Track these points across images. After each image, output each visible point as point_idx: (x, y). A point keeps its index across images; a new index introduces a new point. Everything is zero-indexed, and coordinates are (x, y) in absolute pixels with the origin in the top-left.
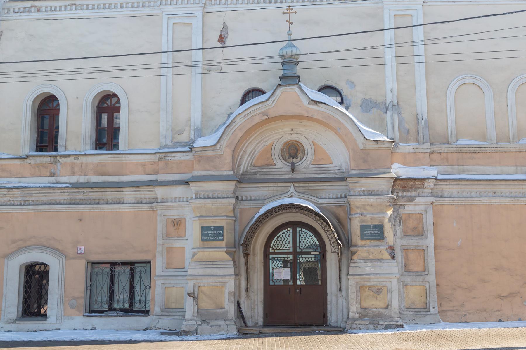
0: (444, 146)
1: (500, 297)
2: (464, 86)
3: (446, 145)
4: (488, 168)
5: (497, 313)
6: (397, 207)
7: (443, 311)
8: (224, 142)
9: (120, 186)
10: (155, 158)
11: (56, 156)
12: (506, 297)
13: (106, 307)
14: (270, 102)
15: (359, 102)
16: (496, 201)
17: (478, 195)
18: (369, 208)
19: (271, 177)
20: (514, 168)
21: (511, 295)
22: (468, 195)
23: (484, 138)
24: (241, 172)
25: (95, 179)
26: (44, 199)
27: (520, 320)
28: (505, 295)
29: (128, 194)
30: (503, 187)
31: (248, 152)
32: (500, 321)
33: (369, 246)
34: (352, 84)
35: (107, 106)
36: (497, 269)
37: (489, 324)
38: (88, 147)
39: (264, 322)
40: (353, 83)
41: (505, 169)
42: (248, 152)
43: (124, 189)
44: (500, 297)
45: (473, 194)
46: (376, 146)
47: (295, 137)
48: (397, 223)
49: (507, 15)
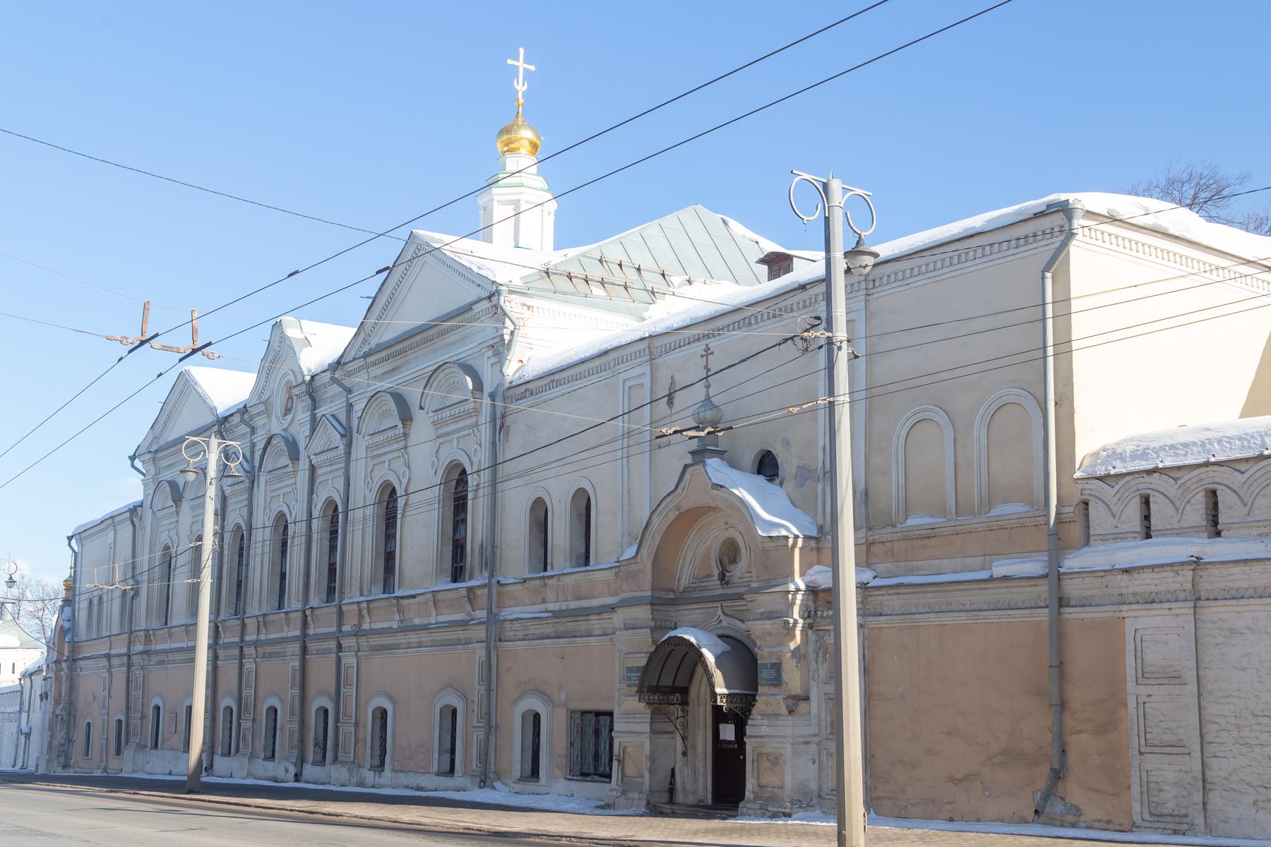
0: (885, 531)
1: (953, 780)
2: (918, 426)
3: (889, 529)
4: (945, 562)
5: (949, 807)
6: (821, 633)
7: (878, 798)
8: (644, 551)
9: (585, 613)
10: (611, 573)
11: (543, 578)
12: (961, 780)
13: (592, 770)
14: (679, 491)
15: (794, 471)
16: (947, 619)
17: (926, 609)
18: (767, 638)
19: (705, 594)
20: (981, 559)
21: (968, 777)
22: (914, 610)
23: (943, 512)
24: (681, 589)
25: (573, 605)
26: (538, 631)
27: (978, 820)
28: (959, 776)
29: (595, 623)
30: (958, 593)
31: (688, 560)
32: (951, 820)
33: (767, 695)
34: (786, 442)
35: (584, 508)
36: (949, 734)
37: (934, 824)
38: (568, 564)
39: (714, 799)
40: (788, 442)
41: (968, 561)
42: (688, 560)
43: (592, 617)
44: (953, 780)
45: (920, 609)
46: (772, 544)
47: (731, 533)
48: (820, 658)
49: (1171, 231)
